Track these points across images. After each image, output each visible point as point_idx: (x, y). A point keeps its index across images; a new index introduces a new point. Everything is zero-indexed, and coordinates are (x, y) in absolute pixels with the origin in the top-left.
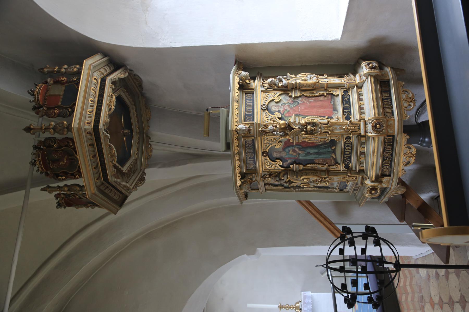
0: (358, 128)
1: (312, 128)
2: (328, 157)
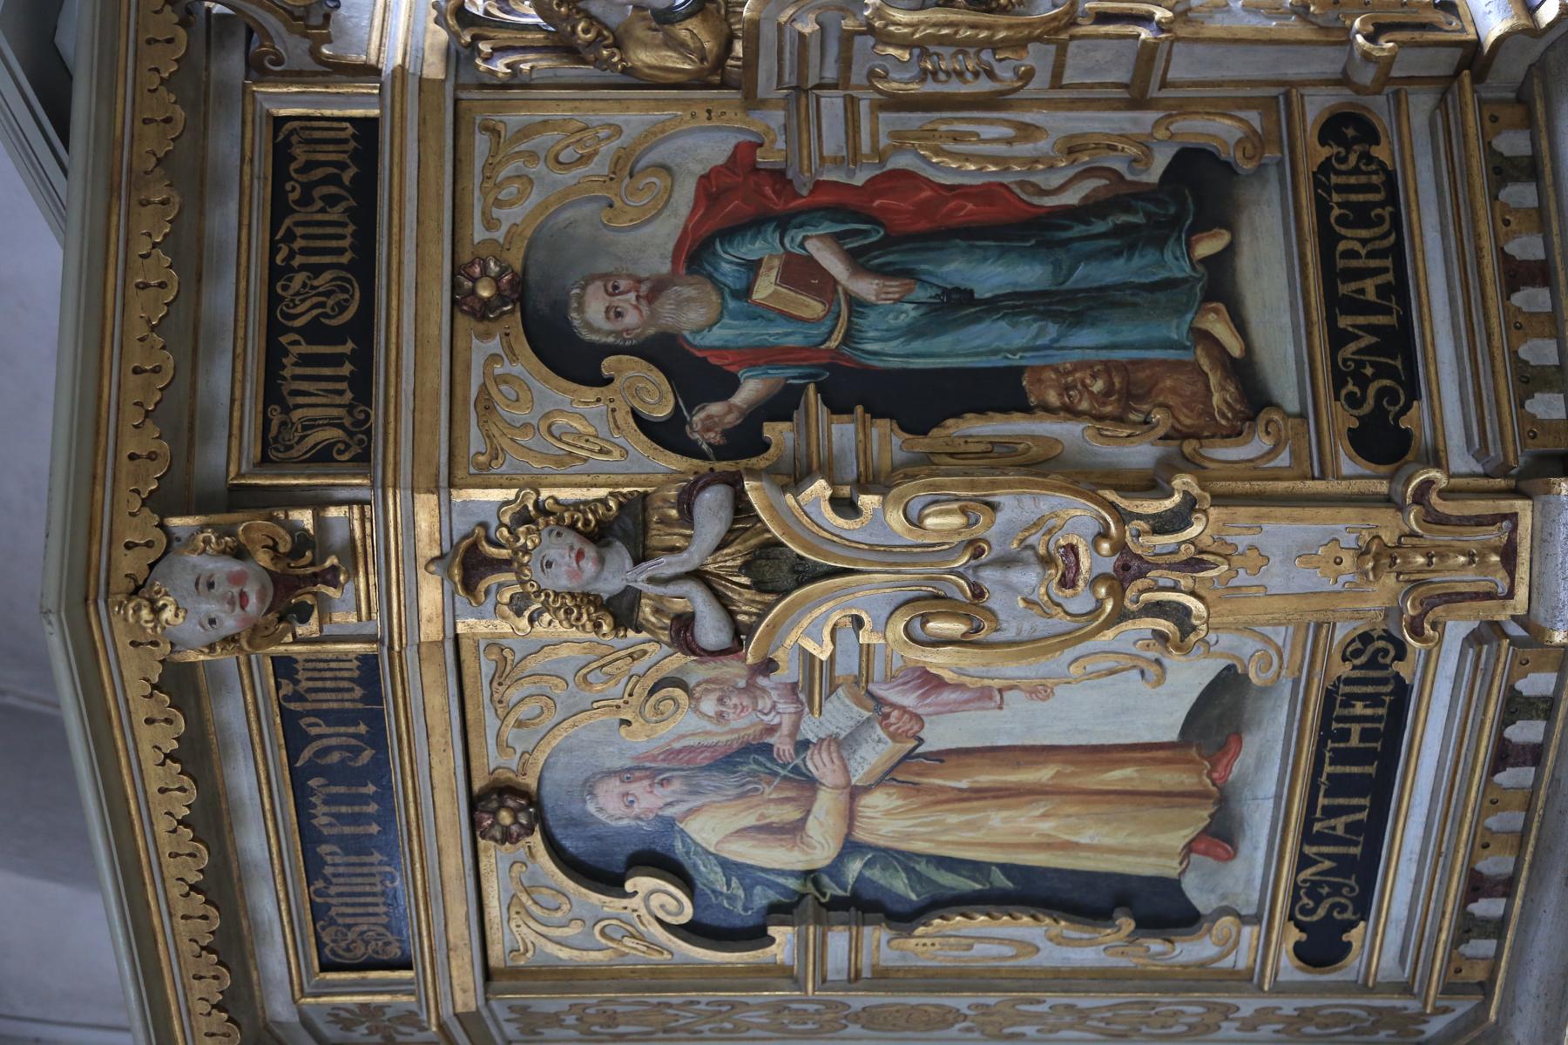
2: (1168, 344)
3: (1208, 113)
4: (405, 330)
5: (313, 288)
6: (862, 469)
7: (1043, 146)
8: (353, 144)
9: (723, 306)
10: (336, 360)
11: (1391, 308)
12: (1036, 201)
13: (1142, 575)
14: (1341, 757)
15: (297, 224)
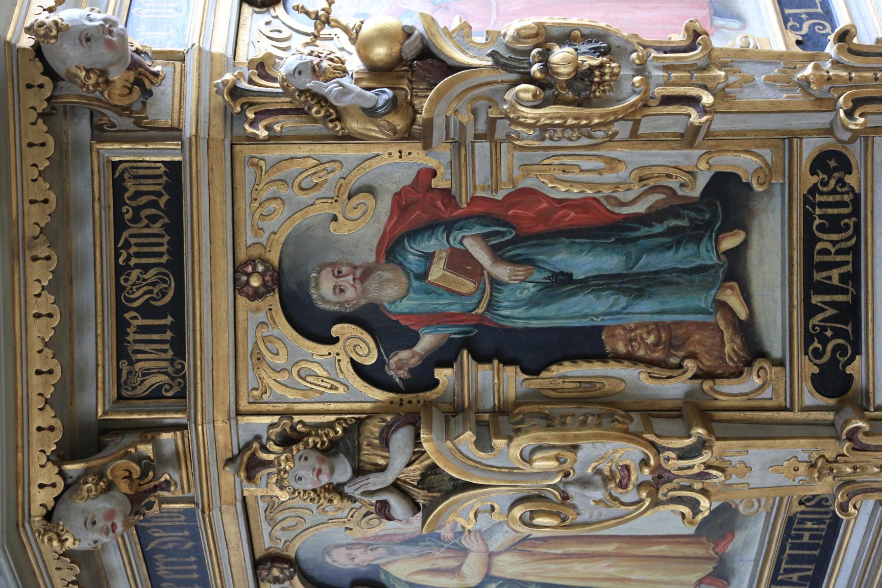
1: (581, 58)
3: (736, 151)
4: (205, 318)
5: (144, 280)
6: (496, 402)
7: (623, 173)
8: (165, 178)
9: (410, 285)
10: (161, 329)
11: (848, 290)
12: (617, 210)
13: (670, 481)
14: (794, 547)
15: (131, 236)
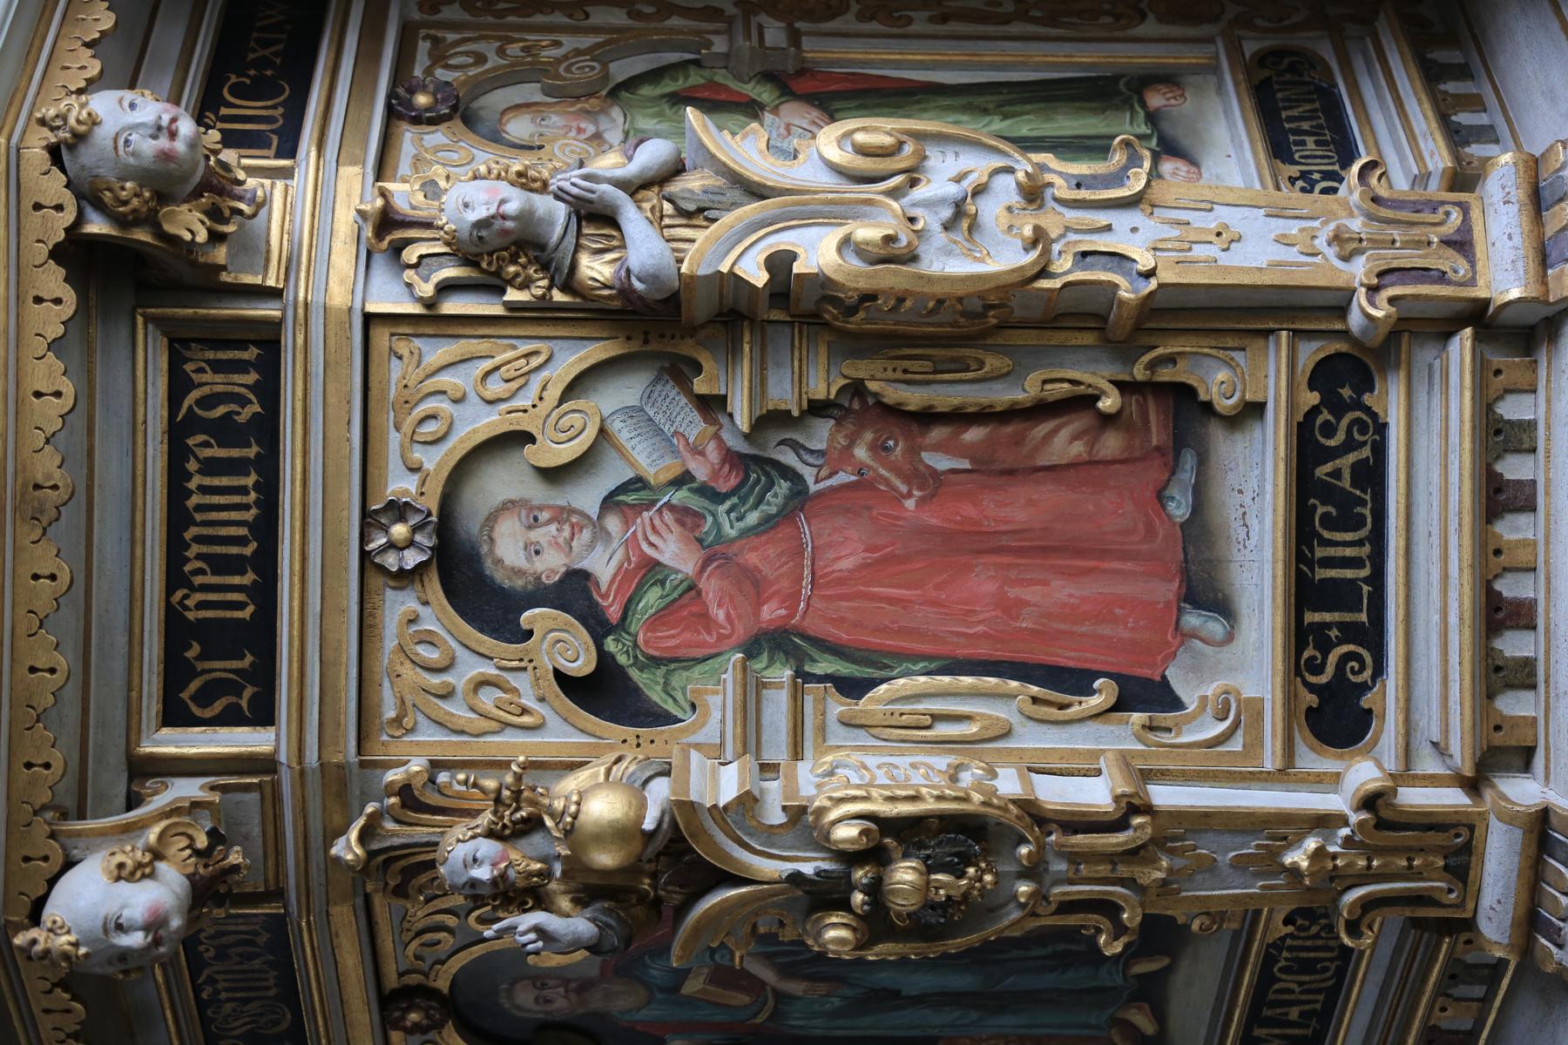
0: (1446, 868)
